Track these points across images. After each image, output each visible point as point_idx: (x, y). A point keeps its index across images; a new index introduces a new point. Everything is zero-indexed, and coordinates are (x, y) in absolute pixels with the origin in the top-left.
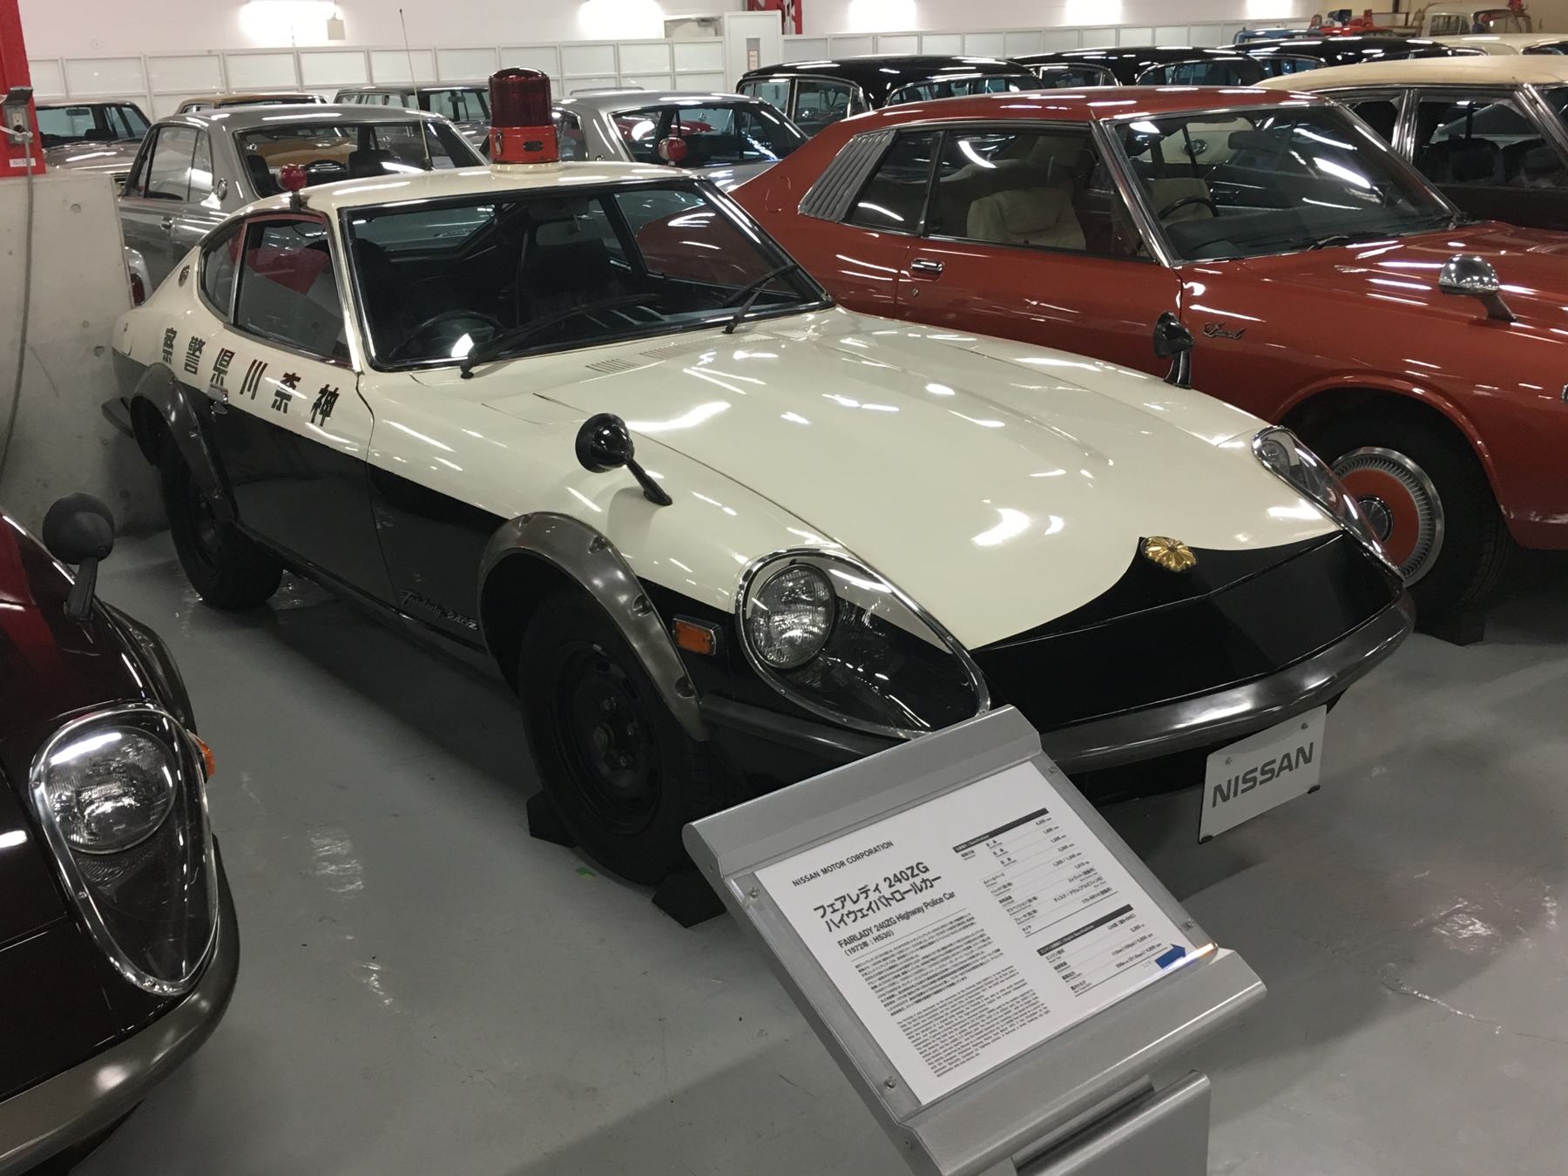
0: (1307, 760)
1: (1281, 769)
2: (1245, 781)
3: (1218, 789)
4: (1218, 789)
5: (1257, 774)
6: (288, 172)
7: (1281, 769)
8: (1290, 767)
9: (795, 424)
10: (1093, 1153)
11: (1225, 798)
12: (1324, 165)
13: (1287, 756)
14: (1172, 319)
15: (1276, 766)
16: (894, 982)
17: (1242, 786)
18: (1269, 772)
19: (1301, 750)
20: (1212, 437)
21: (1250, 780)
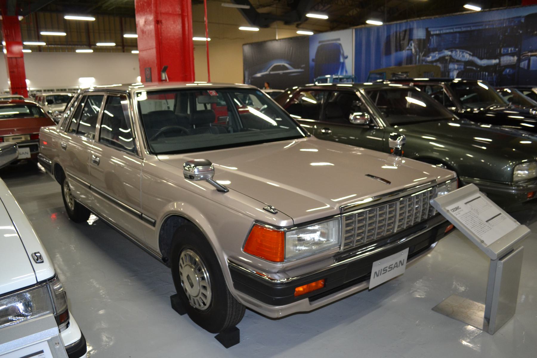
0: (402, 265)
1: (395, 267)
2: (384, 270)
3: (376, 273)
4: (376, 273)
5: (387, 268)
6: (280, 258)
7: (395, 267)
8: (397, 266)
9: (367, 82)
10: (324, 301)
11: (378, 276)
12: (431, 143)
13: (396, 263)
14: (105, 119)
15: (393, 266)
16: (396, 24)
17: (383, 272)
18: (391, 268)
19: (400, 262)
20: (296, 142)
21: (385, 270)
